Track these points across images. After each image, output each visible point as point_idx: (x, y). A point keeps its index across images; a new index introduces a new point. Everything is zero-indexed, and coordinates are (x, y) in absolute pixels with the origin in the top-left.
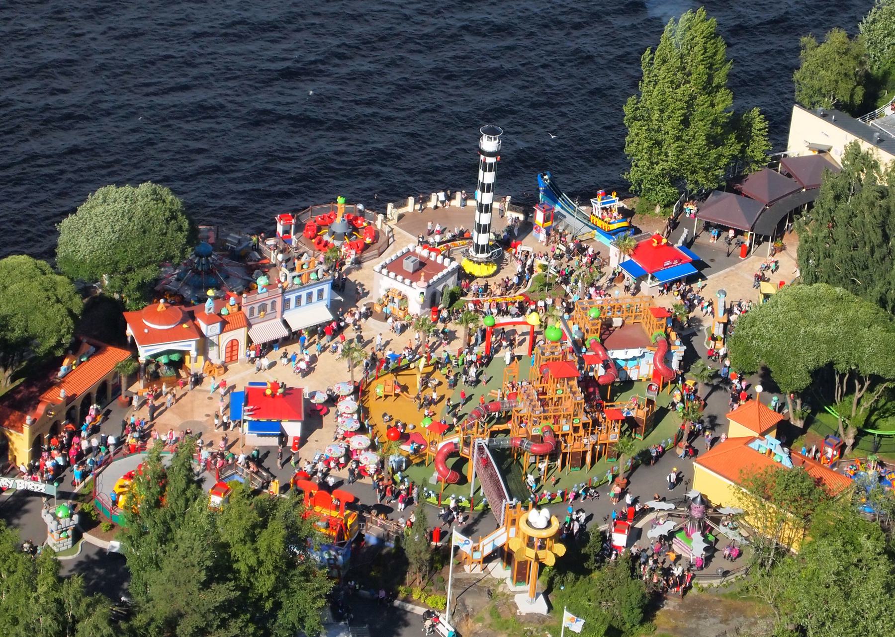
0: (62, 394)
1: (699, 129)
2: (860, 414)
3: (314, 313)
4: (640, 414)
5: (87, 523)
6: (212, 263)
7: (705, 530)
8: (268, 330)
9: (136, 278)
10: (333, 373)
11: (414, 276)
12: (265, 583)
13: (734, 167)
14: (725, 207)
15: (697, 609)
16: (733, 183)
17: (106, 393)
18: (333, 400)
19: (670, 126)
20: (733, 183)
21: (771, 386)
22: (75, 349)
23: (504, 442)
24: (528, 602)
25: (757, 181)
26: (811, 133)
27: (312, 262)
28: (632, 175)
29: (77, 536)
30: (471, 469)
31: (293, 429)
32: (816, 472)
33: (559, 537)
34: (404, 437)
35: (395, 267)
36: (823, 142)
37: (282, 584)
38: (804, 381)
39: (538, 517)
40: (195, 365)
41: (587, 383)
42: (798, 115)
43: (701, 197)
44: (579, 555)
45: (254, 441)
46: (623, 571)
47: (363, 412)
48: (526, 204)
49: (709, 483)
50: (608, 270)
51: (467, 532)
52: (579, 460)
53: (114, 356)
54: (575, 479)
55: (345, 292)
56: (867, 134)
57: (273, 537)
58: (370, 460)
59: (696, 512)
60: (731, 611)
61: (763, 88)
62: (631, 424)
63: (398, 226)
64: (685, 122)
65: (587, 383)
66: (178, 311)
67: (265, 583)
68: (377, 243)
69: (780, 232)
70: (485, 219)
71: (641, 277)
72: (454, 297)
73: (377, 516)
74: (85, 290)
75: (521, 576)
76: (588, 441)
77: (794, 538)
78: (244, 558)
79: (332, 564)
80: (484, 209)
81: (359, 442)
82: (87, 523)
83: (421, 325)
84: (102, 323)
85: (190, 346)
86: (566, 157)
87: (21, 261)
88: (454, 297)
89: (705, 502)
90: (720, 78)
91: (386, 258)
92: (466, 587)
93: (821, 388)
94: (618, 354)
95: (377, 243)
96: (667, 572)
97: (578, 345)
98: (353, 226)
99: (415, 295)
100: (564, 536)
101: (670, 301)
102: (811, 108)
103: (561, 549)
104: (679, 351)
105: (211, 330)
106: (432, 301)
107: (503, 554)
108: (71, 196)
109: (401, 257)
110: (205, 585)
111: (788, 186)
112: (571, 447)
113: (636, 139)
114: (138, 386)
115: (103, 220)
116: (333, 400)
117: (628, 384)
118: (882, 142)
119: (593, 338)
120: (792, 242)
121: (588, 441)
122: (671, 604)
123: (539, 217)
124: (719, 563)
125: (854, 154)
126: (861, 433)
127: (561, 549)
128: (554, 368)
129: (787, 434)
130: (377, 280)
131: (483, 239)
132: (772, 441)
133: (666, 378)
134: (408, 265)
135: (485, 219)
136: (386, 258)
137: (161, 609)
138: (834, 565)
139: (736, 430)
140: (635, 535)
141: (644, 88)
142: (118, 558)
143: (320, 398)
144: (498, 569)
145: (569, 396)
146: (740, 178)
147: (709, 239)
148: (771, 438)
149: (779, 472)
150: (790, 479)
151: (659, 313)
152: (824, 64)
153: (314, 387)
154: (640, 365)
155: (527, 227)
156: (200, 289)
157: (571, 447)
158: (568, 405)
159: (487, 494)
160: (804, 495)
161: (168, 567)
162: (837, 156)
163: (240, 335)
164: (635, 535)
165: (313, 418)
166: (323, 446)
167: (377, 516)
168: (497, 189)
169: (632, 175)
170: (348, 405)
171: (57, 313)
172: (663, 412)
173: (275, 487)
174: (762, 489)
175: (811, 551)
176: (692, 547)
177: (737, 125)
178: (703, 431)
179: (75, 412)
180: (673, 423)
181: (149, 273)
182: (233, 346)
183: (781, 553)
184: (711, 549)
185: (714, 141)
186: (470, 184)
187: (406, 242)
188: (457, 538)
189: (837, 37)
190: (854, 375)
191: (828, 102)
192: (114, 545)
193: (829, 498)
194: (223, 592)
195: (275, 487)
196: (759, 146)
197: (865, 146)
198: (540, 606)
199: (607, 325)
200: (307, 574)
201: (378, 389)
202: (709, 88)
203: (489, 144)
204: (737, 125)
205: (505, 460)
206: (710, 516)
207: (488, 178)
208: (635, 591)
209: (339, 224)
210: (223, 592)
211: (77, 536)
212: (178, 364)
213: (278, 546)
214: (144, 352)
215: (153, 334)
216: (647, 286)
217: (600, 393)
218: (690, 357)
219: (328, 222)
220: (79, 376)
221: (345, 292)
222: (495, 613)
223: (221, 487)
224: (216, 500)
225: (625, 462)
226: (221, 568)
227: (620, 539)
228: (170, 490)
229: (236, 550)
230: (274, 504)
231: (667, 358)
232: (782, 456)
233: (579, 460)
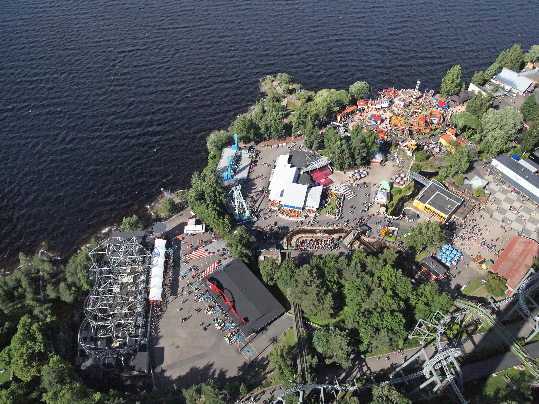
0: (346, 111)
1: (454, 84)
2: (469, 134)
3: (386, 105)
4: (433, 128)
5: (346, 131)
6: (372, 95)
7: (440, 148)
8: (378, 106)
9: (360, 96)
10: (387, 115)
11: (402, 102)
12: (370, 144)
13: (459, 92)
14: (455, 98)
15: (435, 159)
16: (457, 94)
17: (352, 112)
18: (386, 119)
19: (449, 83)
20: (457, 94)
21: (456, 127)
22: (349, 105)
23: (411, 129)
24: (409, 154)
25: (462, 94)
26: (472, 87)
27: (387, 98)
28: (441, 91)
29: (344, 133)
30: (405, 132)
31: (379, 122)
32: (460, 142)
33: (416, 145)
34: (396, 126)
35: (400, 100)
36: (474, 89)
37: (372, 145)
38: (461, 128)
39: (413, 141)
40: (366, 110)
41: (426, 122)
42: (471, 84)
43: (452, 95)
44: (419, 148)
45: (373, 123)
46: (425, 152)
47: (390, 121)
48: (423, 92)
49: (442, 141)
50: (434, 105)
51: (402, 142)
52: (422, 134)
53: (355, 107)
54: (421, 137)
55: (391, 102)
56: (482, 89)
57: (372, 138)
58: (389, 128)
59: (439, 145)
60: (441, 161)
61: (466, 79)
62: (432, 130)
63: (402, 94)
64: (452, 83)
65: (426, 122)
66: (365, 102)
67: (370, 144)
68: (398, 95)
69: (463, 103)
70: (415, 94)
71: (439, 107)
72: (408, 106)
73: (433, 95)
74: (352, 96)
75: (409, 150)
76: (424, 131)
77: (453, 151)
78: (367, 140)
79: (380, 143)
80: (416, 93)
81: (389, 126)
82: (346, 131)
83: (402, 109)
84: (354, 102)
85: (366, 107)
86: (432, 84)
87: (343, 91)
88: (408, 106)
89: (441, 143)
90: (459, 76)
91: (399, 98)
92: (400, 150)
93: (464, 128)
94: (431, 118)
95: (398, 95)
96: (432, 153)
97: (426, 116)
98: (395, 92)
99: (402, 104)
100: (417, 145)
101: (442, 111)
102: (474, 84)
103: (416, 147)
104: (442, 119)
105: (370, 105)
106: (405, 106)
107: (407, 146)
108: (352, 83)
109: (401, 98)
110: (361, 143)
111: (467, 95)
112: (421, 132)
113: (443, 85)
114: (358, 112)
115: (357, 86)
116: (386, 119)
117: (433, 123)
118: (485, 91)
119: (429, 115)
120: (465, 105)
121: (424, 131)
122: (432, 158)
123: (424, 95)
124: (441, 153)
125: (479, 92)
126: (469, 137)
127: (416, 147)
128: (422, 119)
129: (456, 135)
130: (397, 101)
131: (415, 97)
132: (454, 136)
133: (439, 123)
134: (402, 100)
135: (415, 94)
136: (399, 98)
137: (354, 145)
138: (458, 157)
139: (448, 133)
140: (428, 147)
141: (446, 76)
142: (349, 137)
143: (384, 118)
144: (406, 148)
145: (423, 123)
146: (459, 93)
147: (451, 102)
148: (454, 136)
149: (454, 141)
150: (455, 142)
151: (440, 113)
152: (478, 76)
153: (384, 117)
154: (435, 121)
155: (421, 96)
156: (369, 98)
157: (421, 132)
158: (422, 125)
159: (406, 137)
160: (457, 145)
161: (356, 139)
162: (476, 92)
163: (374, 107)
164: (428, 147)
165: (382, 121)
166: (383, 125)
167: (433, 95)
168: (419, 90)
169: (441, 91)
170: (388, 120)
171: (347, 99)
172: (437, 129)
173: (374, 130)
174: (451, 143)
175: (455, 154)
176: (437, 150)
177: (460, 85)
178: (443, 132)
179: (347, 115)
180: (438, 130)
181: (362, 95)
182: (372, 108)
183: (451, 153)
184: (440, 151)
185: (456, 87)
186: (414, 88)
187: (402, 96)
188: (400, 143)
189: (481, 72)
190: (470, 128)
191: (477, 83)
192: (349, 135)
193: (460, 146)
194: (363, 144)
195: (374, 130)
196: (463, 89)
197: (482, 91)
198: (411, 155)
199: (431, 114)
200: (376, 144)
201: (393, 118)
202: (457, 78)
203: (419, 82)
204: (460, 85)
205: (411, 132)
206: (441, 146)
207: (417, 88)
208: (426, 155)
209: (392, 92)
210: (363, 144)
211: (344, 133)
212: (364, 110)
213: (373, 139)
214: (359, 107)
215: (361, 104)
216: (439, 108)
217: (427, 124)
218: (444, 121)
219: (390, 91)
220: (349, 109)
221: (391, 102)
222: (404, 154)
223: (366, 129)
224: (365, 131)
225: (429, 135)
226: (364, 141)
227: (426, 147)
228: (359, 128)
229: (366, 139)
230: (374, 132)
231: (440, 120)
232: (455, 139)
233: (422, 134)
